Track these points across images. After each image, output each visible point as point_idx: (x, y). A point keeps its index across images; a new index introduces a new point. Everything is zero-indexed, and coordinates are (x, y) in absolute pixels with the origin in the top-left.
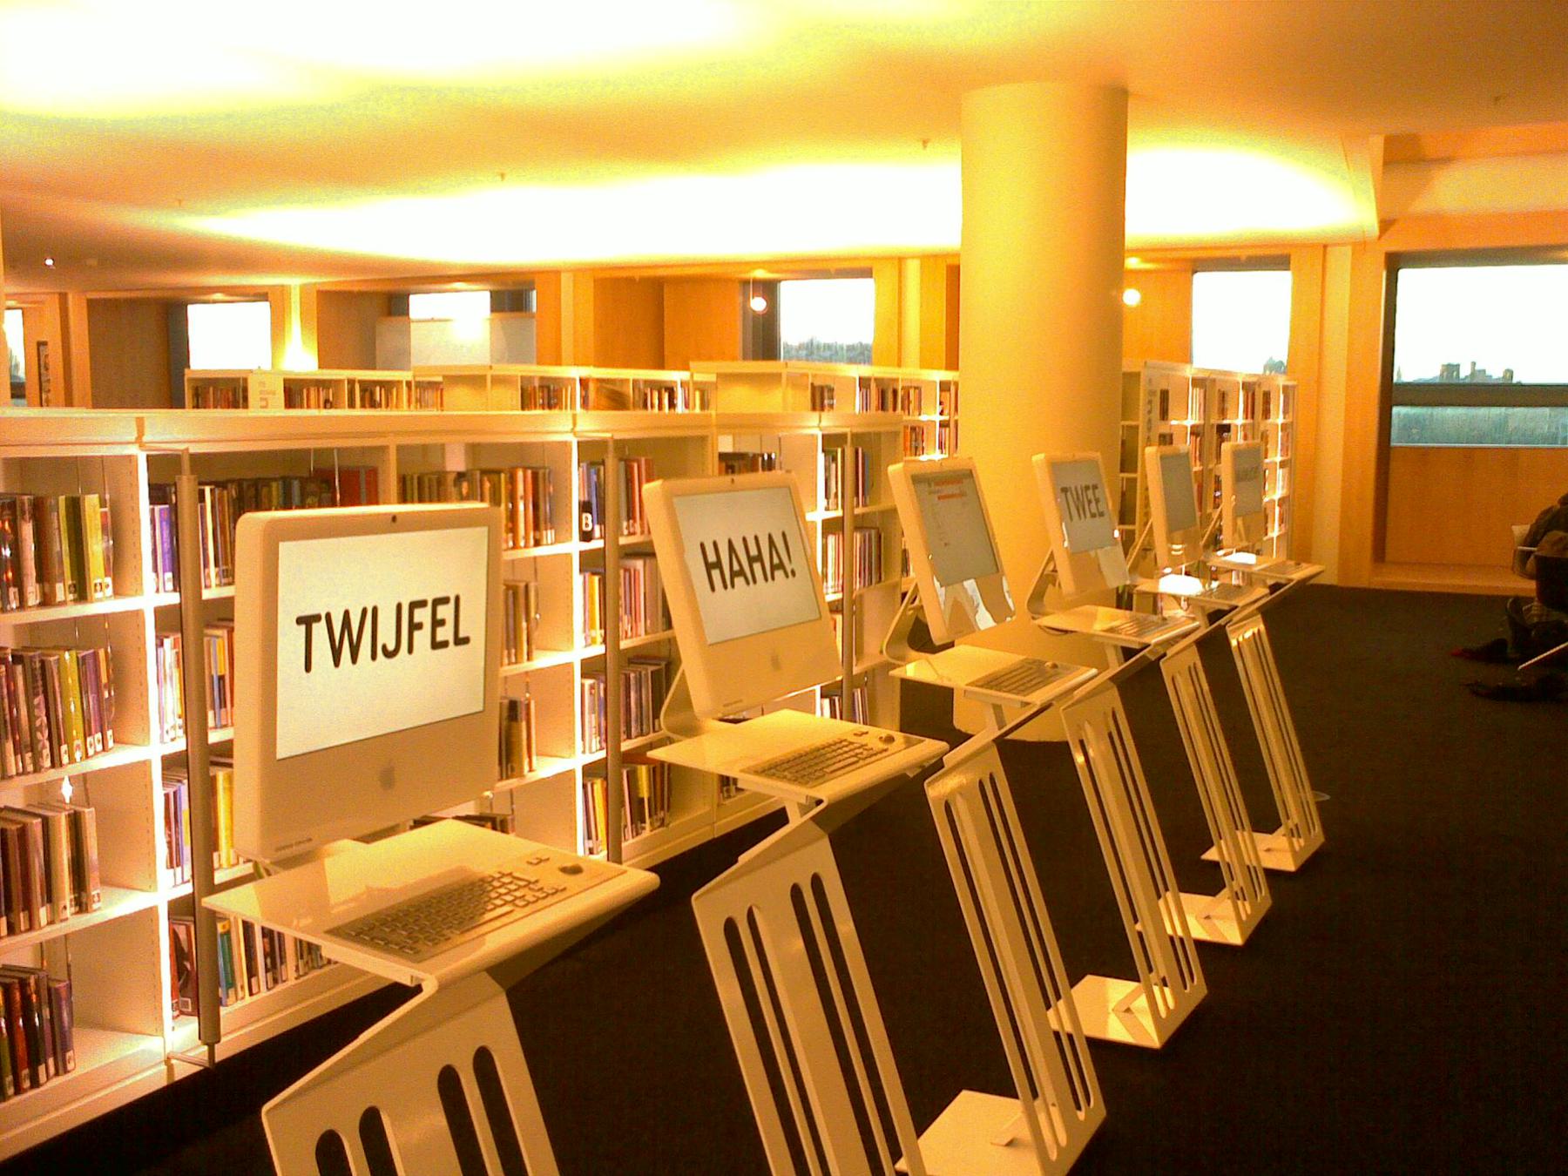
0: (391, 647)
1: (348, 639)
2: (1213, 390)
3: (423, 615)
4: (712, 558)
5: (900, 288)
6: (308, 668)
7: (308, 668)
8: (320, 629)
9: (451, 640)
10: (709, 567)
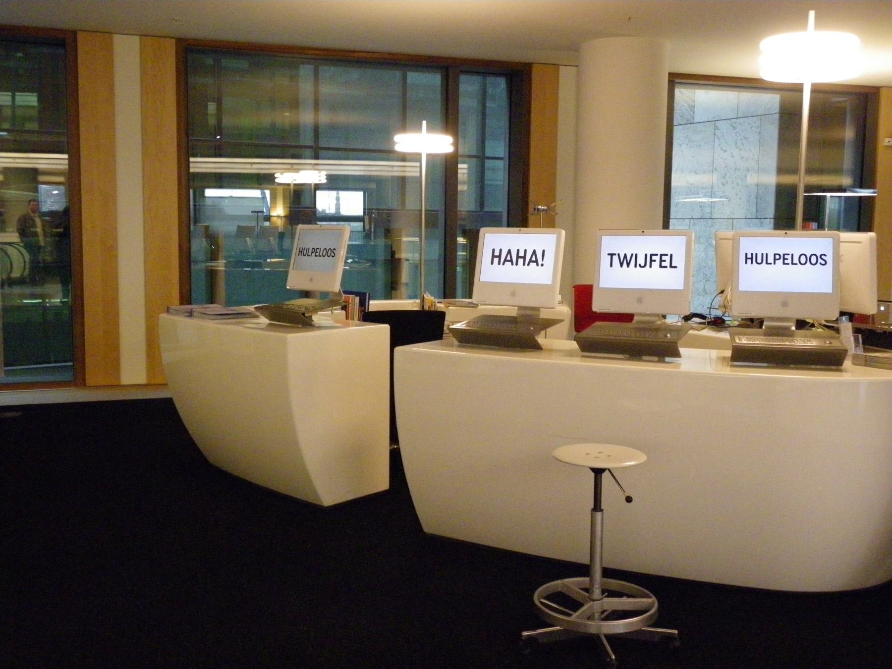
0: (643, 264)
1: (625, 261)
2: (311, 317)
3: (657, 258)
4: (497, 253)
5: (862, 166)
6: (611, 266)
7: (611, 266)
8: (615, 258)
9: (668, 265)
10: (493, 256)
